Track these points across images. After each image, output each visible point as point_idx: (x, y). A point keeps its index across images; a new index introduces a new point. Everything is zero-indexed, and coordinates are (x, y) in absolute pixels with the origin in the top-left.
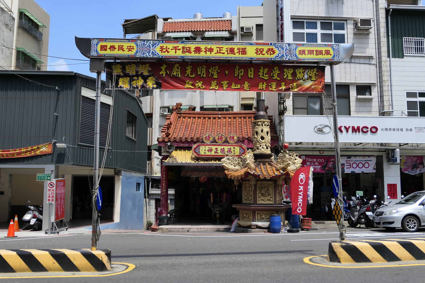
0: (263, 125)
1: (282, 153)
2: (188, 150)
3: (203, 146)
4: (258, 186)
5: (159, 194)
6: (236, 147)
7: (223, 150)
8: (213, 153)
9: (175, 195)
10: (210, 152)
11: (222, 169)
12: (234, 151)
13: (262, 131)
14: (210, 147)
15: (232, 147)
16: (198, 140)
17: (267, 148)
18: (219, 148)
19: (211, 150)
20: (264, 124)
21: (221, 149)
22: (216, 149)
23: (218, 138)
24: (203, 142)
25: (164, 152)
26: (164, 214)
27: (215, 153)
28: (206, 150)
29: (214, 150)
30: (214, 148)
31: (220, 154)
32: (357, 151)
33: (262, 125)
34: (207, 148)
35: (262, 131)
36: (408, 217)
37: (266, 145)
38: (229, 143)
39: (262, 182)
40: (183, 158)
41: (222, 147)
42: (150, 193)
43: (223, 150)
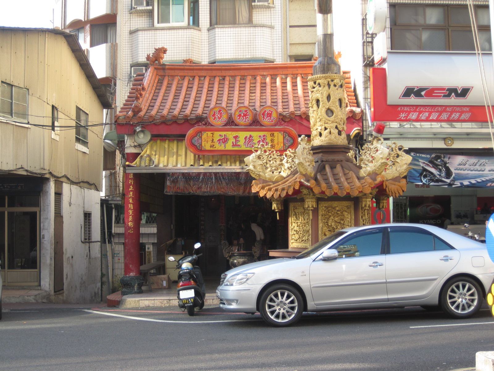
0: (332, 86)
1: (370, 142)
2: (178, 141)
3: (209, 133)
4: (320, 213)
5: (154, 234)
6: (276, 134)
7: (249, 140)
8: (229, 146)
9: (159, 235)
10: (223, 145)
11: (247, 179)
12: (272, 141)
13: (329, 98)
14: (223, 133)
15: (267, 134)
16: (200, 120)
17: (340, 133)
18: (242, 135)
19: (225, 140)
20: (332, 84)
21: (246, 138)
22: (236, 137)
23: (240, 115)
24: (207, 124)
25: (131, 146)
26: (132, 271)
27: (233, 145)
28: (216, 140)
29: (231, 140)
30: (230, 135)
31: (243, 148)
32: (429, 29)
33: (329, 85)
34: (217, 135)
35: (329, 98)
36: (261, 301)
37: (336, 127)
38: (261, 125)
39: (330, 203)
40: (173, 160)
41: (248, 134)
42: (113, 232)
43: (249, 140)
